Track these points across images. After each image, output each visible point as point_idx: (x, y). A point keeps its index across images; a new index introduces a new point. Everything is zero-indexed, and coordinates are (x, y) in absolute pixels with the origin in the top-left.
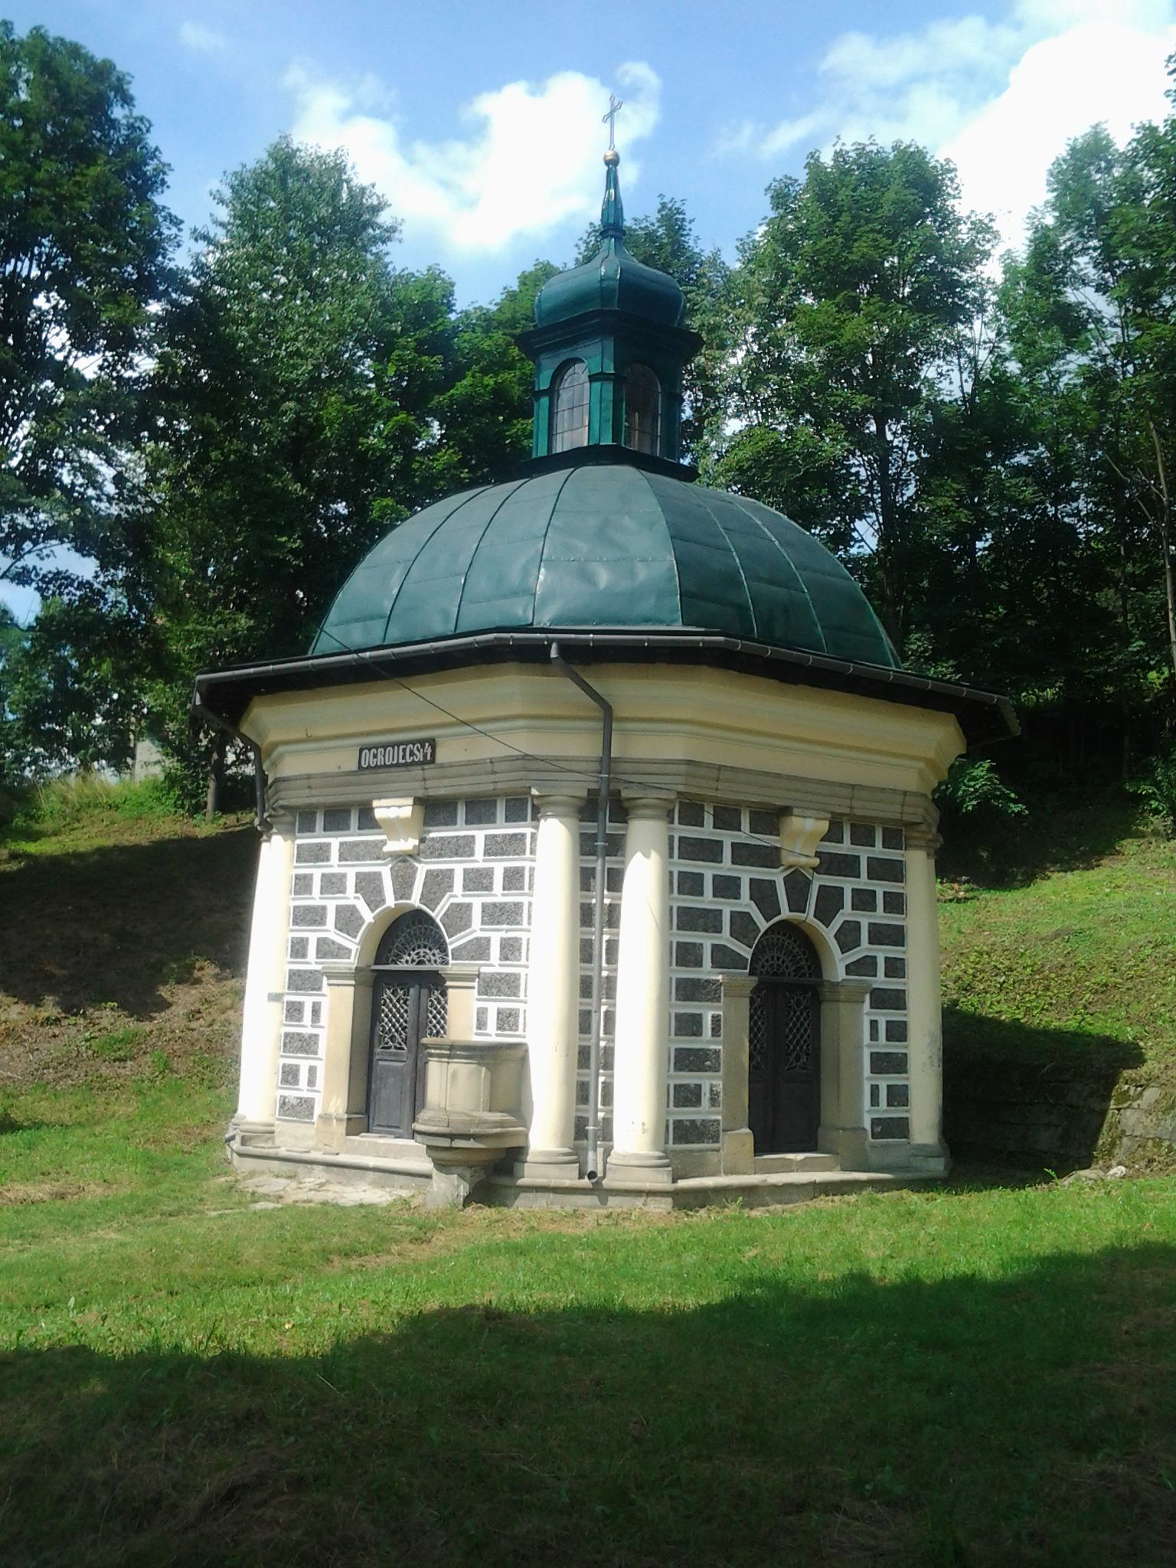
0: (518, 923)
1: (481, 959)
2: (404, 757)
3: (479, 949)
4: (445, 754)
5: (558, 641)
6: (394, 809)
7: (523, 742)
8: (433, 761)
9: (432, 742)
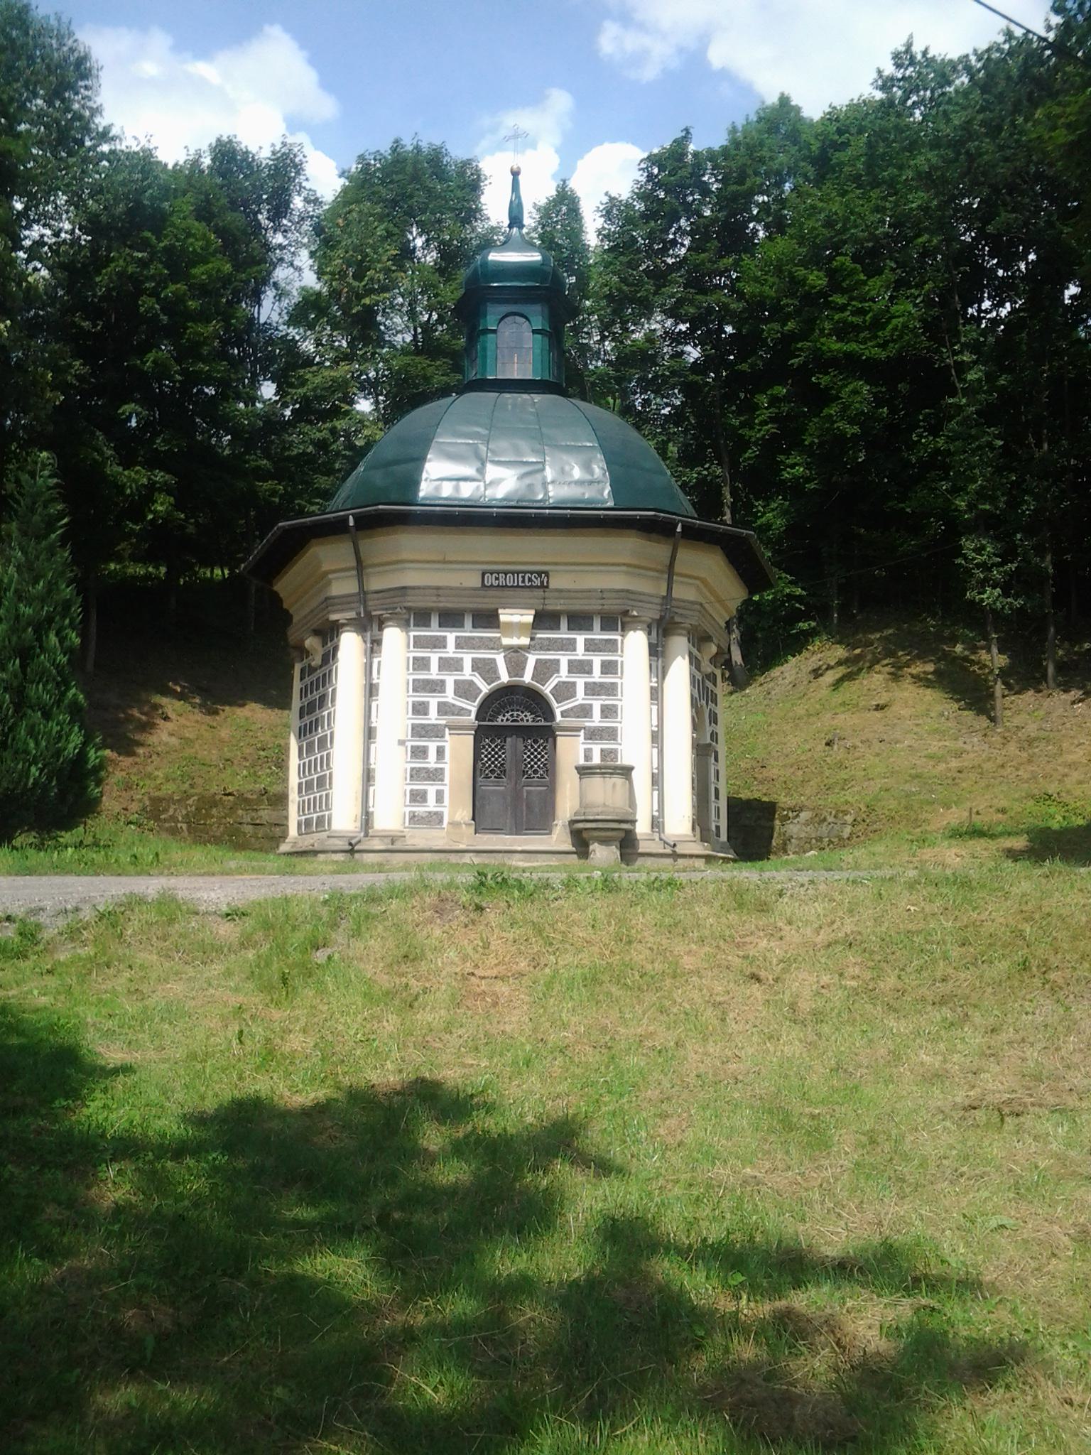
4: (555, 583)
6: (517, 616)
7: (618, 581)
9: (547, 574)
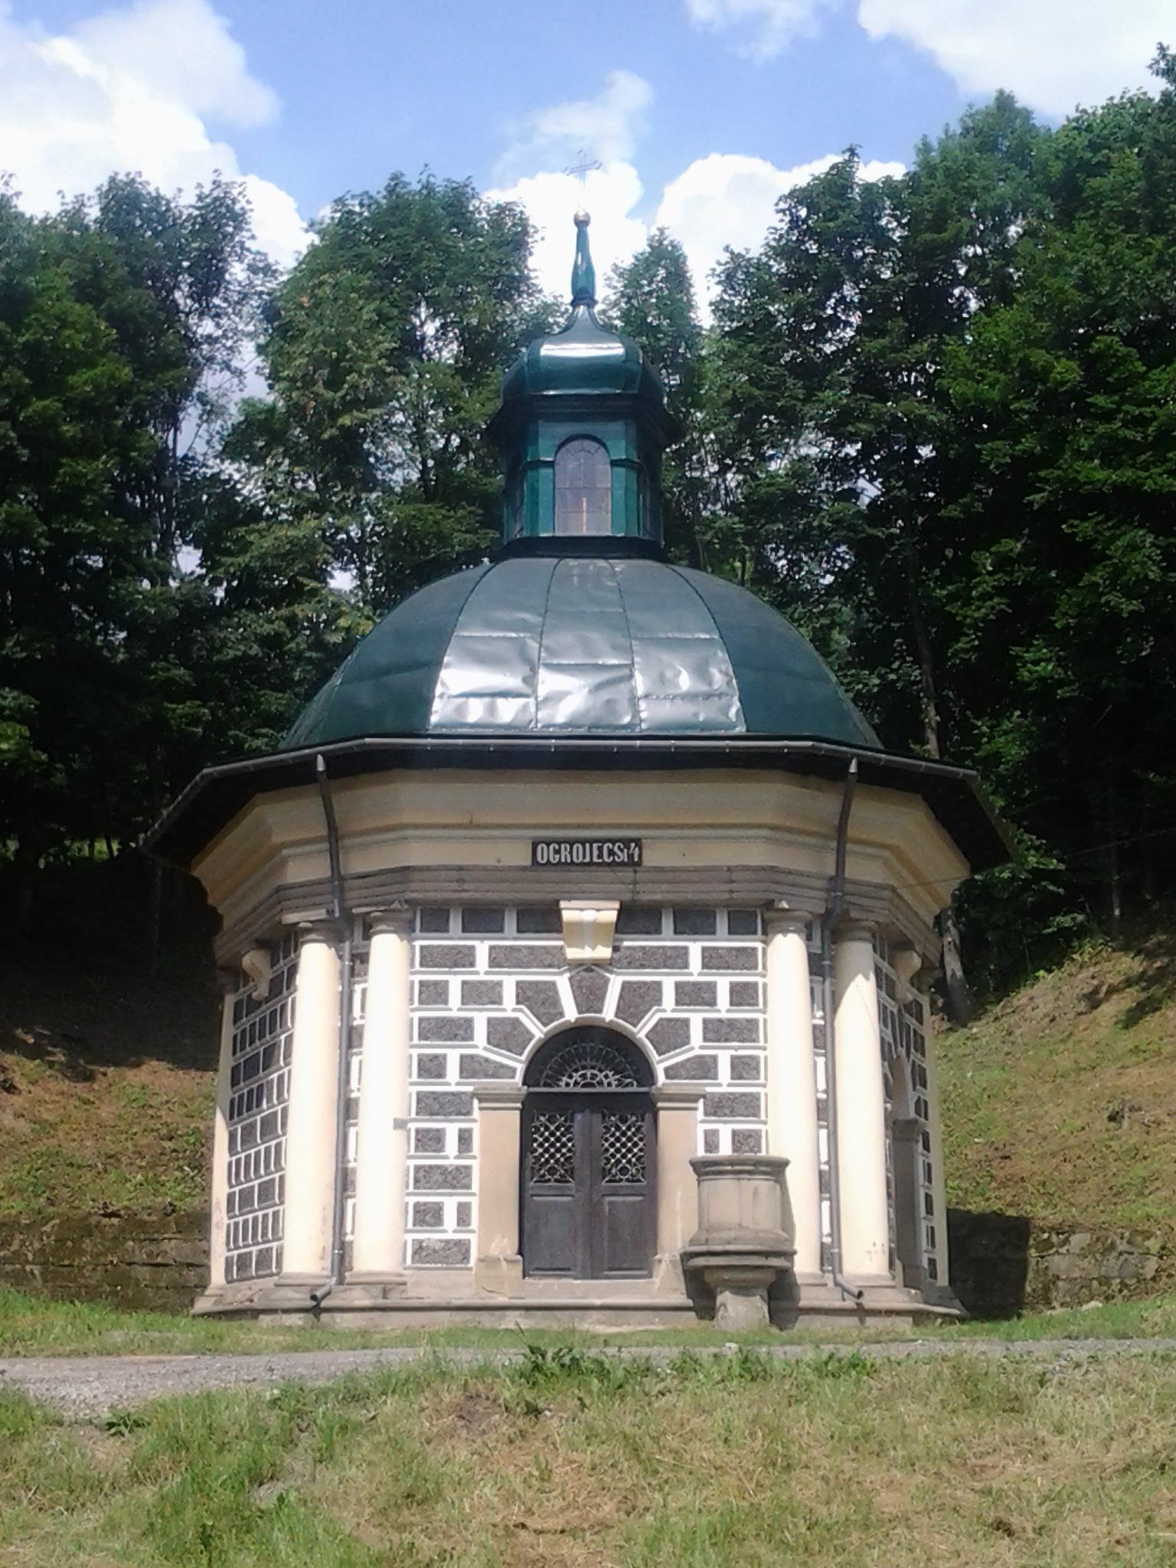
0: (754, 1041)
1: (706, 1078)
2: (600, 856)
3: (705, 1068)
4: (653, 857)
5: (323, 754)
7: (756, 854)
8: (639, 863)
9: (638, 842)
